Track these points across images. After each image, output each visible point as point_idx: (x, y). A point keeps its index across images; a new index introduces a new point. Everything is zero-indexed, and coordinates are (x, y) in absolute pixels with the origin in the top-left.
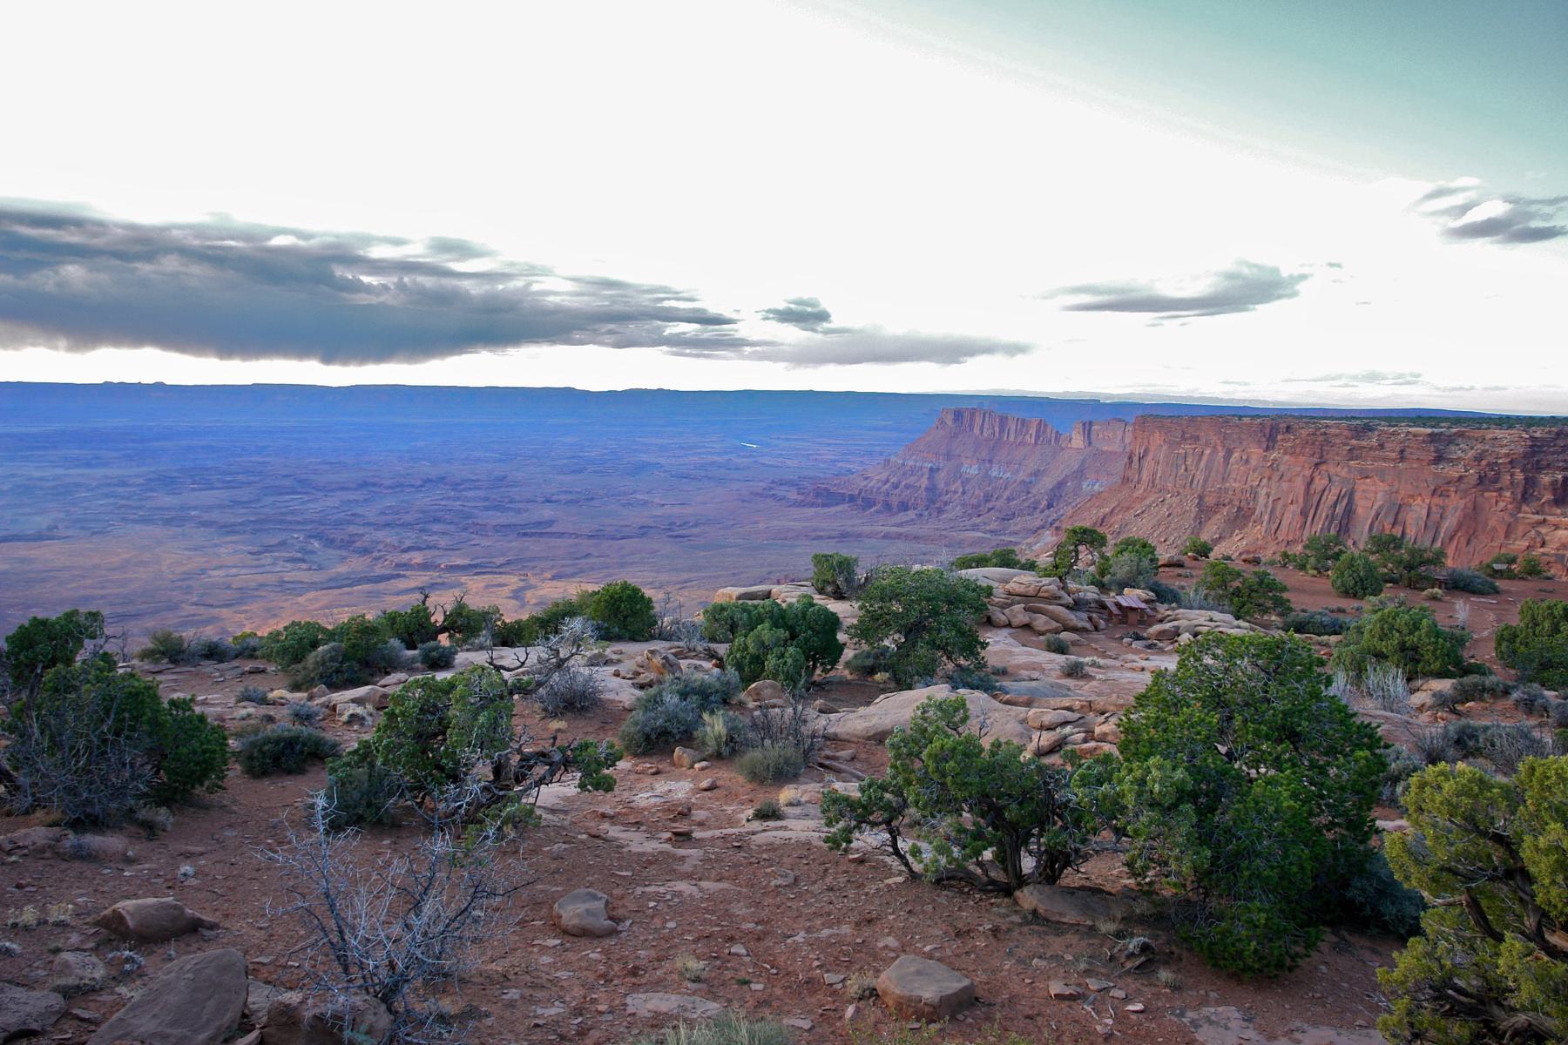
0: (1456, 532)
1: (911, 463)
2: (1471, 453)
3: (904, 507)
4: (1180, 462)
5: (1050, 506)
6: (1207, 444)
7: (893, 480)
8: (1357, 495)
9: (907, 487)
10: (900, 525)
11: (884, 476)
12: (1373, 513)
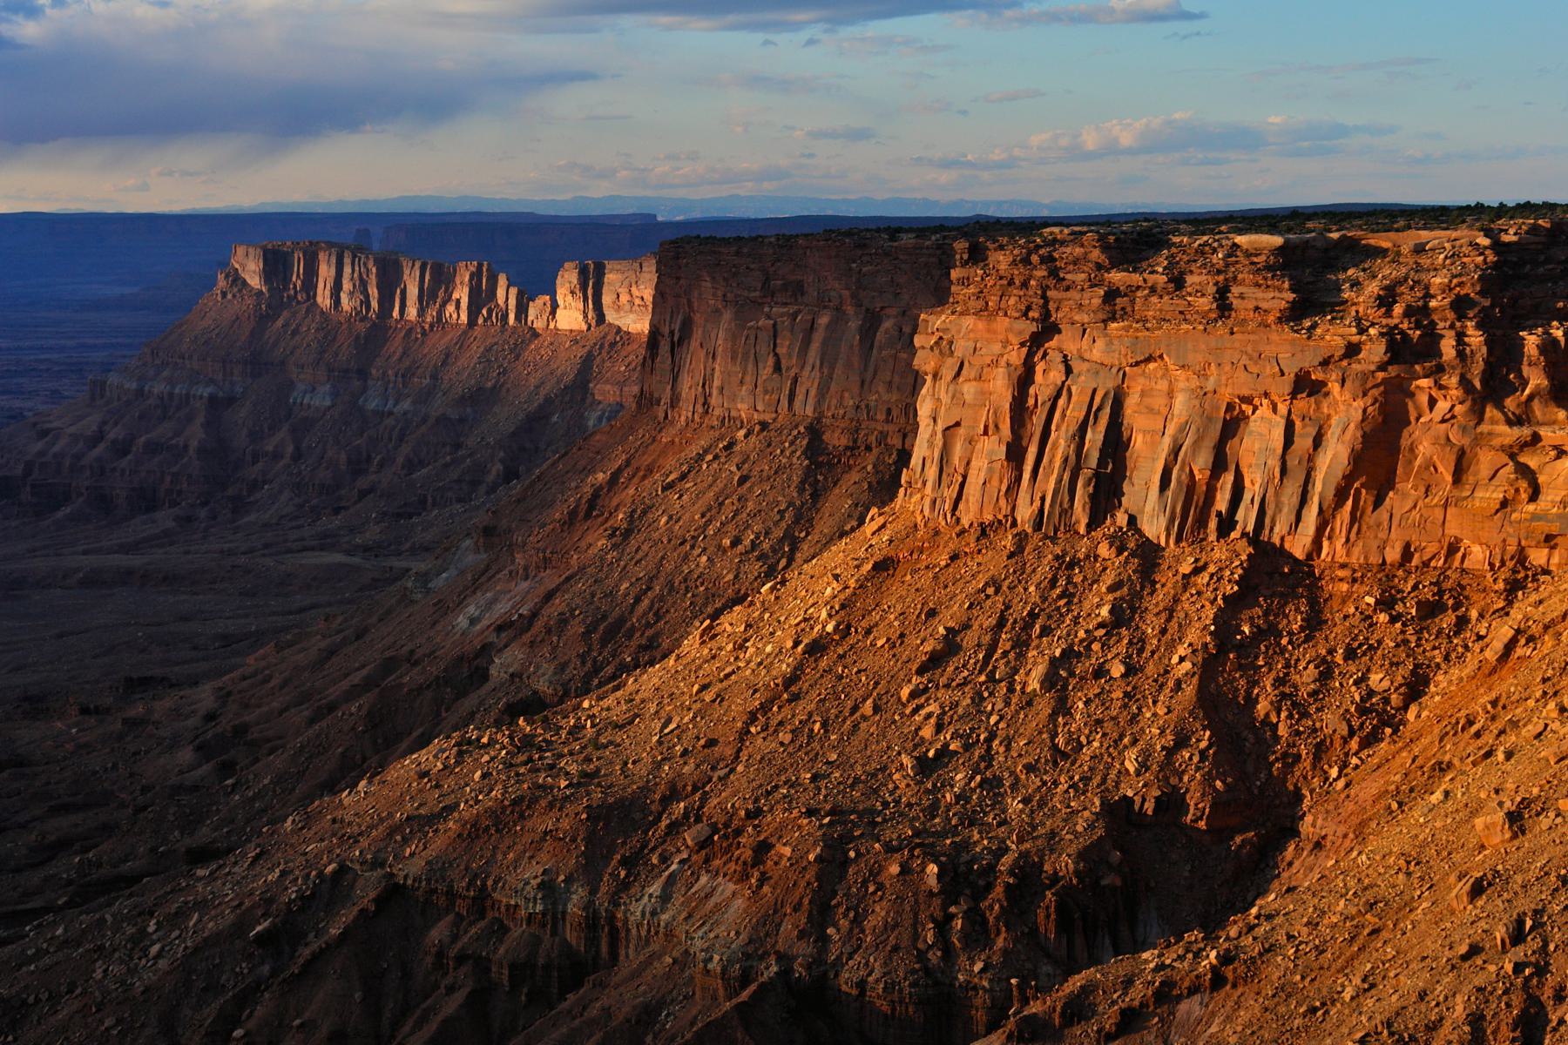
0: (1349, 478)
1: (159, 388)
2: (1373, 288)
3: (146, 501)
4: (763, 348)
5: (510, 475)
6: (822, 304)
7: (115, 433)
8: (1131, 403)
9: (153, 448)
10: (125, 549)
11: (91, 423)
12: (1167, 442)
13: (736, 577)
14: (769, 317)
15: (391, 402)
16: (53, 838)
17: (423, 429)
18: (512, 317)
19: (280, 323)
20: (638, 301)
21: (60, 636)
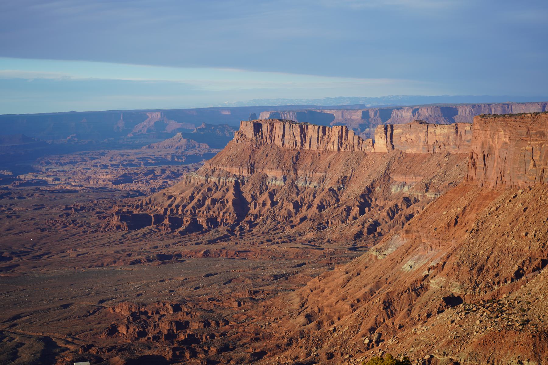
1: (214, 179)
13: (530, 248)
14: (530, 145)
15: (308, 183)
16: (259, 350)
17: (323, 193)
18: (356, 147)
19: (261, 152)
20: (409, 141)
21: (207, 276)
